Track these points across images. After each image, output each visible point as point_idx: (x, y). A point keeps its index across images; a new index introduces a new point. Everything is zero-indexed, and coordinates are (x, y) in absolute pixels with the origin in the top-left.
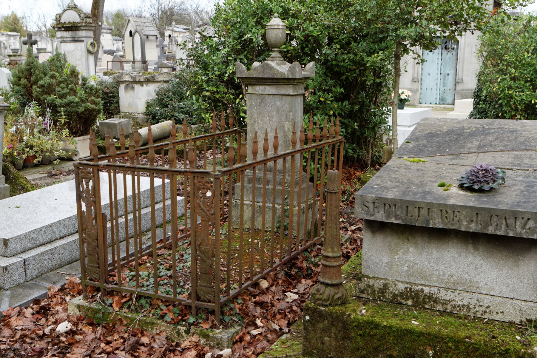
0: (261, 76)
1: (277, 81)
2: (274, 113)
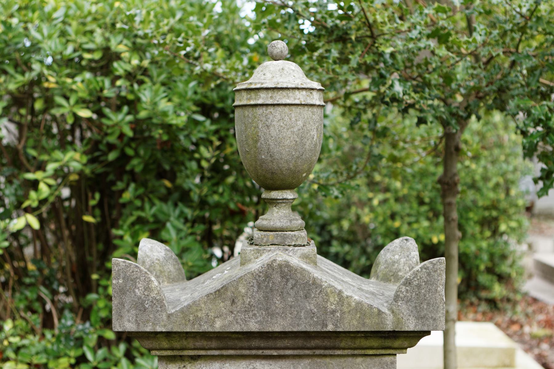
0: (253, 326)
1: (327, 343)
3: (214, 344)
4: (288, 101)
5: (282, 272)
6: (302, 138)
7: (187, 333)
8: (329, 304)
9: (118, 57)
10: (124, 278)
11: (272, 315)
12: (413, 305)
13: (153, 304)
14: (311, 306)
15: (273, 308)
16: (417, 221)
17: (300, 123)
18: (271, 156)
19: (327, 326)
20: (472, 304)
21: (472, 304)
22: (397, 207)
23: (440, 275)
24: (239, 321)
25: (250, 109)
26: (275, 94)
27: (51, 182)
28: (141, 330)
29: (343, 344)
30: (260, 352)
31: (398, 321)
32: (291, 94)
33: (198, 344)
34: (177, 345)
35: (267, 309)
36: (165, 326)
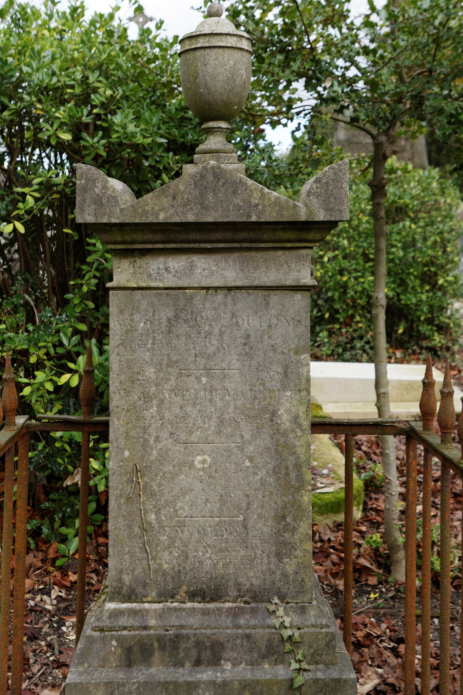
0: (190, 218)
1: (252, 235)
2: (233, 361)
3: (158, 237)
4: (222, 44)
5: (214, 173)
6: (233, 75)
7: (137, 224)
8: (253, 199)
9: (95, 90)
10: (86, 179)
11: (206, 208)
12: (323, 199)
13: (109, 200)
14: (238, 201)
15: (207, 202)
16: (362, 277)
17: (231, 62)
18: (208, 89)
19: (251, 217)
20: (414, 352)
21: (414, 352)
22: (346, 264)
23: (344, 174)
24: (179, 213)
25: (192, 53)
26: (211, 39)
27: (37, 195)
28: (99, 221)
29: (265, 237)
30: (197, 245)
31: (310, 213)
32: (224, 39)
33: (146, 237)
34: (128, 238)
35: (202, 204)
36: (118, 218)
